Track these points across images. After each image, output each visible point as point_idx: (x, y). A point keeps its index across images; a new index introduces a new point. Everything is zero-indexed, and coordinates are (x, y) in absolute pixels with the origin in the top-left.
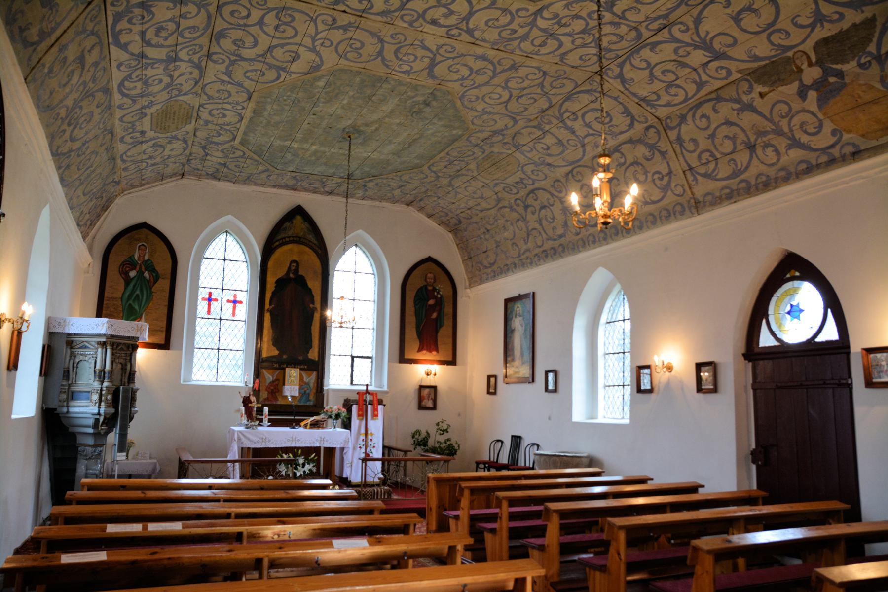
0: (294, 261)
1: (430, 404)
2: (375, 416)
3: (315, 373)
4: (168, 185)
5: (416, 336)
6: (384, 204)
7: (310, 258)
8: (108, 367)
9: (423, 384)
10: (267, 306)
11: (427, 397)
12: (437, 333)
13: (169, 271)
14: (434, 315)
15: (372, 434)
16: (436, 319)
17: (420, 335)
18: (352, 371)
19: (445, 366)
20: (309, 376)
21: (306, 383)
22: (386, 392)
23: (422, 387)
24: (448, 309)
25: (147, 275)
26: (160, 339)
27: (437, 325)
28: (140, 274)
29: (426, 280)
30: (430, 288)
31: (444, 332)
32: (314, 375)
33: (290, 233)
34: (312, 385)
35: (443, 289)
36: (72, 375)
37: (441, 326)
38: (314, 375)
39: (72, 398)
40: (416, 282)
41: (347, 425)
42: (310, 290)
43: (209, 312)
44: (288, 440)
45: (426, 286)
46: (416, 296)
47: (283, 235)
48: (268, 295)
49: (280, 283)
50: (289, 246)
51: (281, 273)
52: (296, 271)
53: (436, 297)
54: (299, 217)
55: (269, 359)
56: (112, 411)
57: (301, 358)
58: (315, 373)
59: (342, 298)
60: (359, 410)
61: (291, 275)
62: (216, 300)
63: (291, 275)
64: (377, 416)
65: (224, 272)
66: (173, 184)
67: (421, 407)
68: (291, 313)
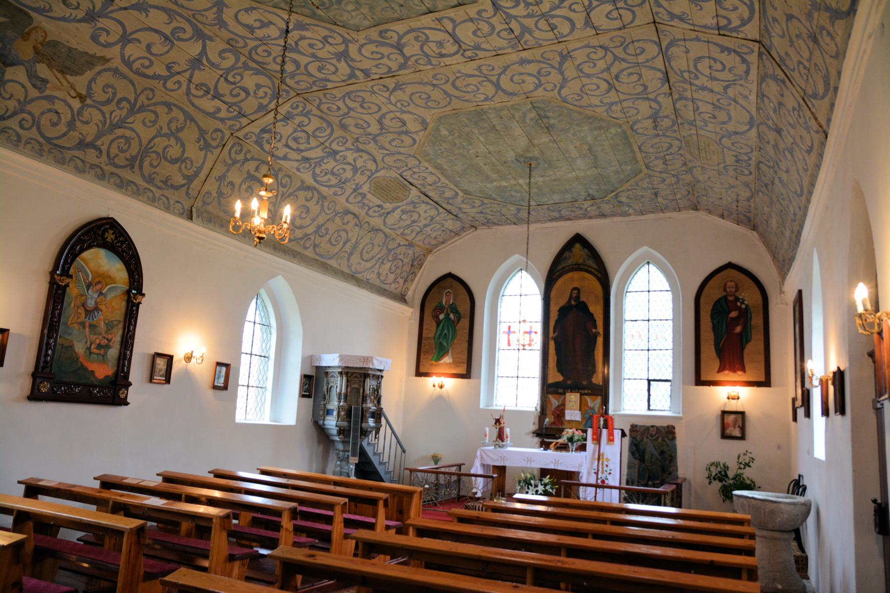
0: (575, 289)
1: (737, 433)
2: (611, 440)
3: (599, 398)
4: (466, 238)
5: (714, 354)
6: (668, 214)
7: (592, 283)
8: (343, 391)
9: (727, 409)
10: (551, 334)
11: (733, 424)
12: (742, 349)
13: (469, 311)
14: (738, 329)
15: (608, 460)
16: (741, 334)
17: (720, 352)
18: (649, 395)
19: (755, 388)
20: (594, 401)
21: (590, 408)
22: (680, 418)
23: (724, 413)
24: (757, 320)
25: (452, 316)
26: (462, 370)
27: (743, 339)
28: (447, 315)
29: (725, 290)
30: (731, 298)
31: (753, 348)
32: (599, 400)
33: (570, 262)
34: (596, 410)
35: (750, 297)
36: (327, 397)
37: (747, 342)
38: (599, 400)
39: (328, 414)
40: (714, 293)
41: (583, 448)
42: (592, 315)
43: (509, 344)
44: (551, 462)
45: (725, 298)
46: (712, 310)
47: (563, 265)
48: (552, 324)
49: (564, 311)
50: (570, 275)
51: (563, 301)
52: (578, 297)
53: (739, 308)
54: (578, 245)
55: (556, 385)
56: (345, 424)
57: (585, 383)
58: (599, 398)
59: (524, 321)
60: (594, 434)
61: (573, 303)
62: (514, 332)
63: (573, 303)
64: (613, 440)
65: (517, 309)
66: (469, 236)
67: (724, 436)
68: (578, 342)
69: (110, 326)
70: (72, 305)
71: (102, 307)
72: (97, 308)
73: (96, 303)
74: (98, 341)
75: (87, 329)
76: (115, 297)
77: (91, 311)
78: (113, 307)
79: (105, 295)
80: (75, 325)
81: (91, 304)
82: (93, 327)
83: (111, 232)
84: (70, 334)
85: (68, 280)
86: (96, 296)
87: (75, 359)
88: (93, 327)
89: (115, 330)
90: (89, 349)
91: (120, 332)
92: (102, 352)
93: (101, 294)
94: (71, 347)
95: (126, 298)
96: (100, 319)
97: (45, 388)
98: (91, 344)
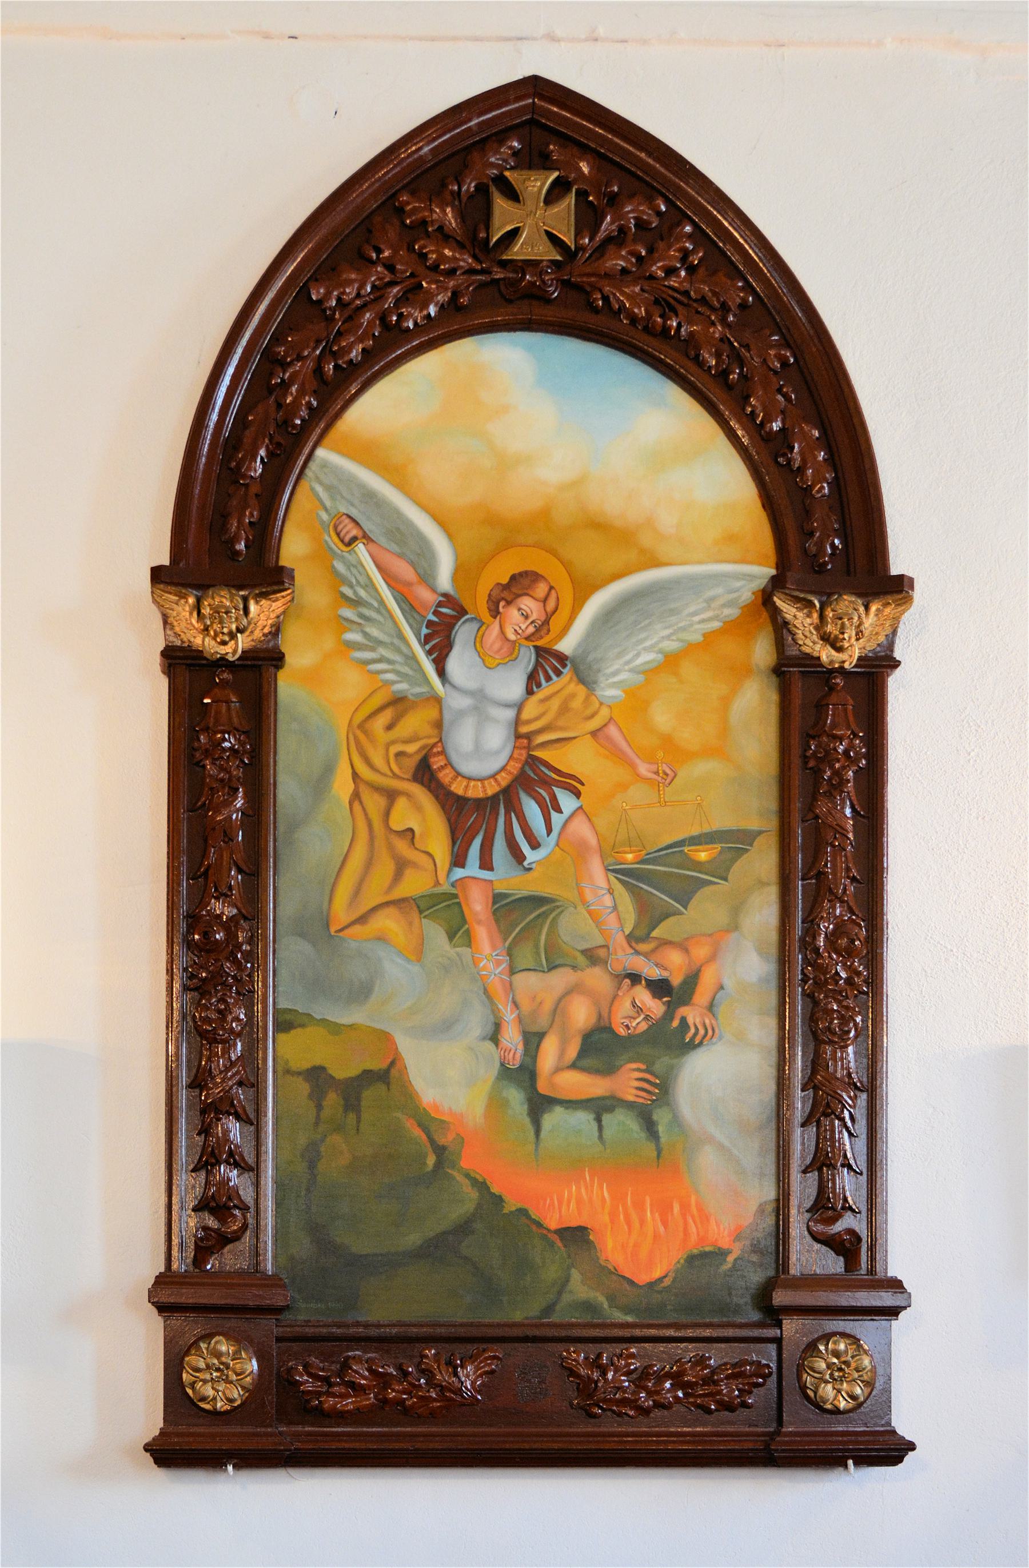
69: (661, 882)
70: (342, 786)
71: (577, 758)
72: (534, 776)
73: (522, 737)
74: (581, 1015)
75: (482, 934)
76: (671, 662)
77: (486, 806)
78: (668, 742)
79: (581, 670)
80: (388, 922)
81: (480, 753)
82: (524, 916)
83: (537, 184)
84: (361, 992)
85: (262, 612)
86: (511, 684)
87: (439, 1151)
88: (524, 916)
89: (705, 910)
90: (523, 1074)
91: (763, 914)
92: (628, 1081)
93: (547, 663)
94: (385, 1077)
95: (762, 651)
96: (566, 856)
97: (227, 1375)
98: (533, 1040)
